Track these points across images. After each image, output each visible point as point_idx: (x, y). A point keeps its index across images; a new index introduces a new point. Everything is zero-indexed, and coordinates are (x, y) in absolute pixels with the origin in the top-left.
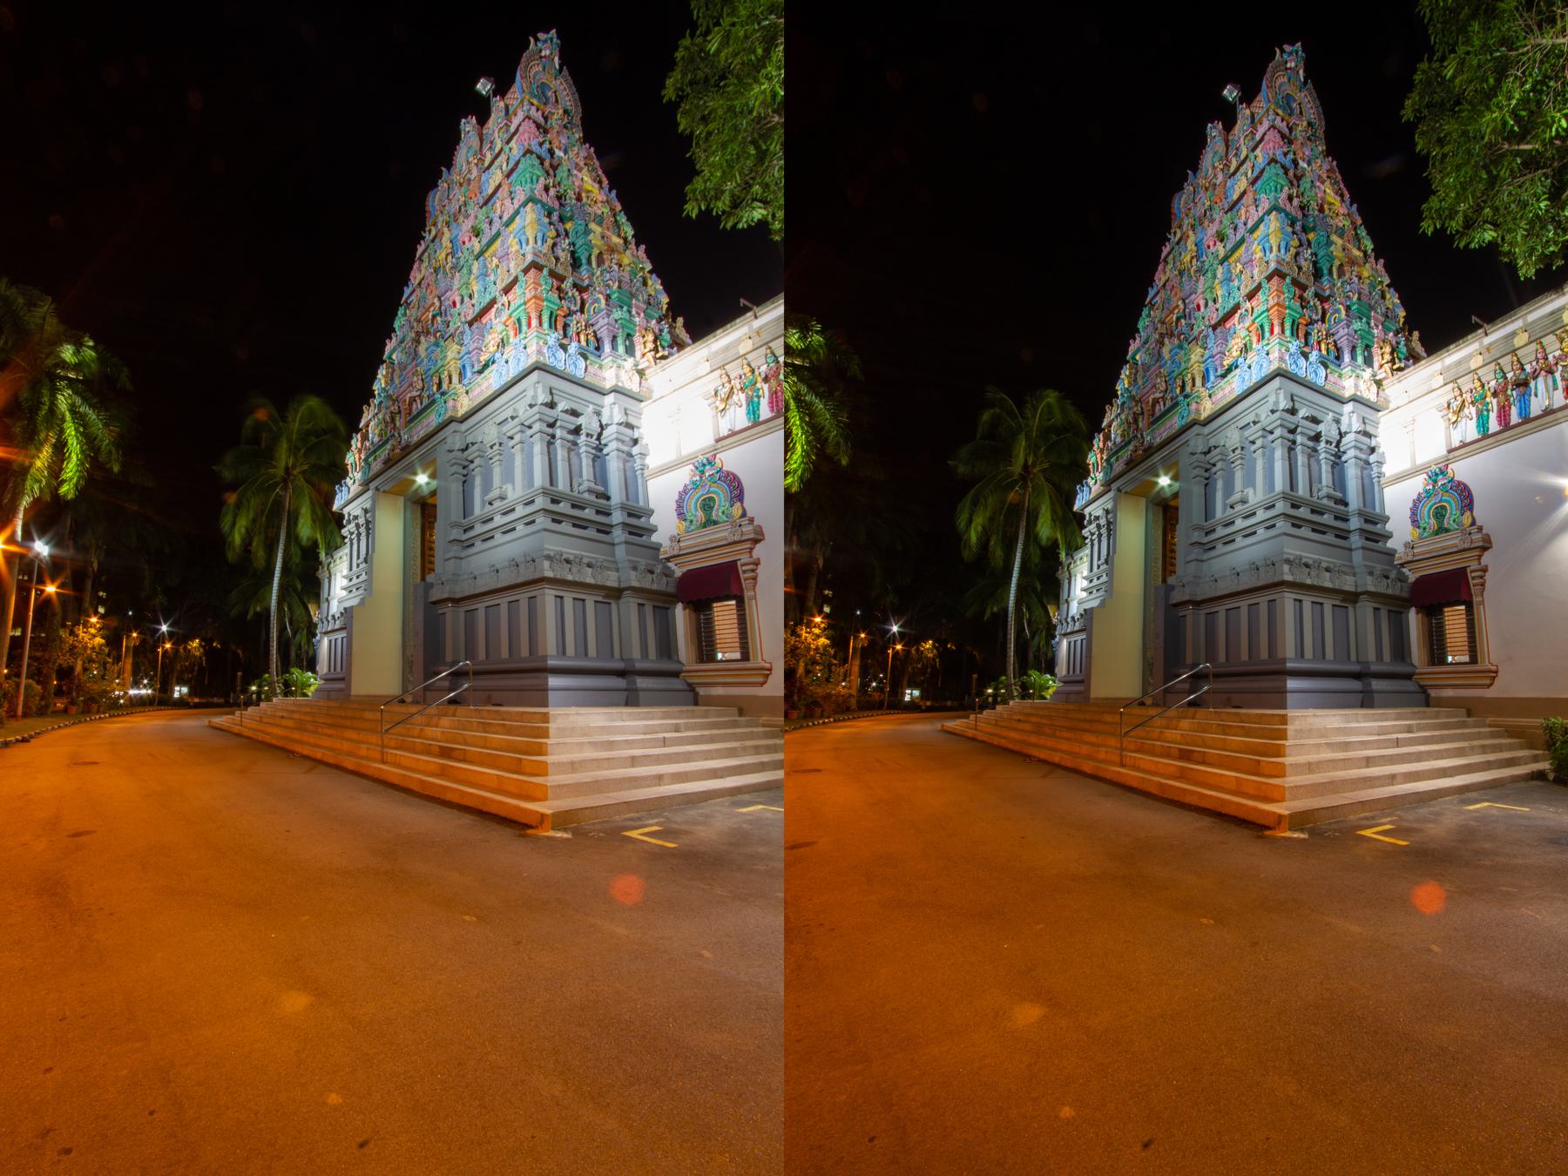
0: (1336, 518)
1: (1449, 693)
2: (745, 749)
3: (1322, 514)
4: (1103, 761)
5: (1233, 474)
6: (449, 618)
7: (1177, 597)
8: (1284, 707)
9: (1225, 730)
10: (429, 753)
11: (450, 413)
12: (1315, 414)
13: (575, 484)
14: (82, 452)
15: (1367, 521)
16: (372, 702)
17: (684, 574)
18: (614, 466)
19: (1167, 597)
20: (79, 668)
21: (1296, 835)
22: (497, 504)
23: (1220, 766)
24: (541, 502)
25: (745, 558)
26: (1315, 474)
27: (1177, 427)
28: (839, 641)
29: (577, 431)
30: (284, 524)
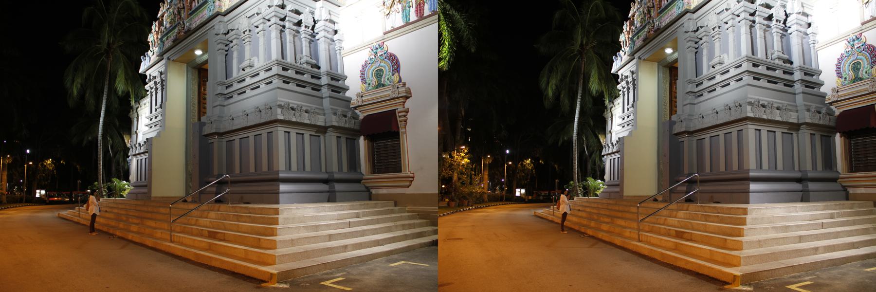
0: (312, 77)
1: (862, 191)
2: (396, 226)
3: (303, 74)
4: (626, 238)
5: (244, 48)
6: (686, 144)
7: (207, 130)
8: (277, 203)
9: (707, 218)
10: (201, 236)
11: (217, 10)
12: (298, 8)
13: (298, 60)
14: (452, 40)
15: (332, 79)
16: (167, 201)
17: (365, 117)
18: (795, 41)
19: (201, 130)
20: (455, 177)
21: (745, 288)
22: (248, 70)
23: (235, 242)
24: (276, 70)
25: (400, 108)
26: (298, 48)
27: (676, 14)
28: (475, 159)
29: (770, 18)
30: (107, 82)
